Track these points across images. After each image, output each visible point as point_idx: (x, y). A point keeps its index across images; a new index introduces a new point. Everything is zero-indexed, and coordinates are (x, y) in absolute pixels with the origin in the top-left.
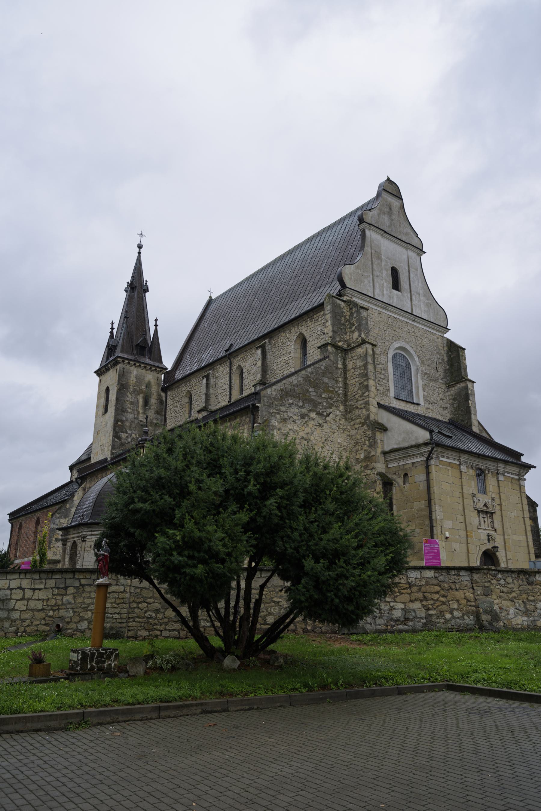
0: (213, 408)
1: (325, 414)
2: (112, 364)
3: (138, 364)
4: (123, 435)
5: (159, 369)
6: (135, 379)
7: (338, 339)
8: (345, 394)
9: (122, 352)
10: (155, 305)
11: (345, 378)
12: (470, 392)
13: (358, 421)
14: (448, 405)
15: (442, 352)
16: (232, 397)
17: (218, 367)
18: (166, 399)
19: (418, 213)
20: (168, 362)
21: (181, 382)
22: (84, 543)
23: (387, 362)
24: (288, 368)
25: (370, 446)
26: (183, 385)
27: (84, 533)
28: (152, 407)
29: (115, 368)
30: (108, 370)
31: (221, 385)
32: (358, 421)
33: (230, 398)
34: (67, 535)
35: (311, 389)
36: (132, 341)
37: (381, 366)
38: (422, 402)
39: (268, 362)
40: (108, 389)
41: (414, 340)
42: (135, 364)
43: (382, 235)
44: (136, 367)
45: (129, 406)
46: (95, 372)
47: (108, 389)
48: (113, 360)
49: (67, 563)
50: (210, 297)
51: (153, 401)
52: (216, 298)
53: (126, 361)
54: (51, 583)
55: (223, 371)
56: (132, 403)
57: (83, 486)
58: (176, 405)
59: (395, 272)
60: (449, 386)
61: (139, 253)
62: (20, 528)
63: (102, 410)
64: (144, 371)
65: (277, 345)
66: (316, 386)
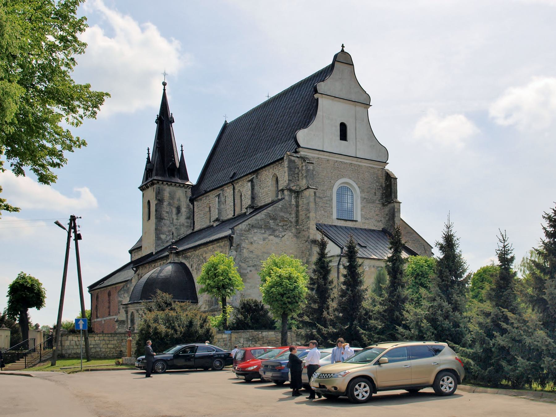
1: (281, 236)
3: (170, 183)
4: (163, 237)
6: (168, 195)
7: (293, 185)
8: (297, 222)
9: (157, 175)
11: (298, 211)
12: (396, 210)
13: (303, 239)
14: (383, 219)
15: (381, 180)
18: (194, 208)
19: (366, 74)
20: (193, 178)
23: (331, 195)
25: (310, 255)
29: (153, 187)
30: (148, 187)
32: (303, 239)
35: (270, 221)
36: (164, 165)
37: (326, 198)
38: (359, 219)
39: (256, 191)
40: (149, 202)
41: (356, 175)
43: (332, 100)
44: (169, 185)
47: (149, 202)
48: (151, 181)
50: (226, 121)
51: (184, 210)
54: (116, 338)
55: (228, 191)
57: (137, 272)
58: (200, 212)
59: (343, 128)
60: (384, 205)
61: (164, 90)
62: (97, 297)
63: (147, 217)
64: (174, 188)
66: (274, 219)
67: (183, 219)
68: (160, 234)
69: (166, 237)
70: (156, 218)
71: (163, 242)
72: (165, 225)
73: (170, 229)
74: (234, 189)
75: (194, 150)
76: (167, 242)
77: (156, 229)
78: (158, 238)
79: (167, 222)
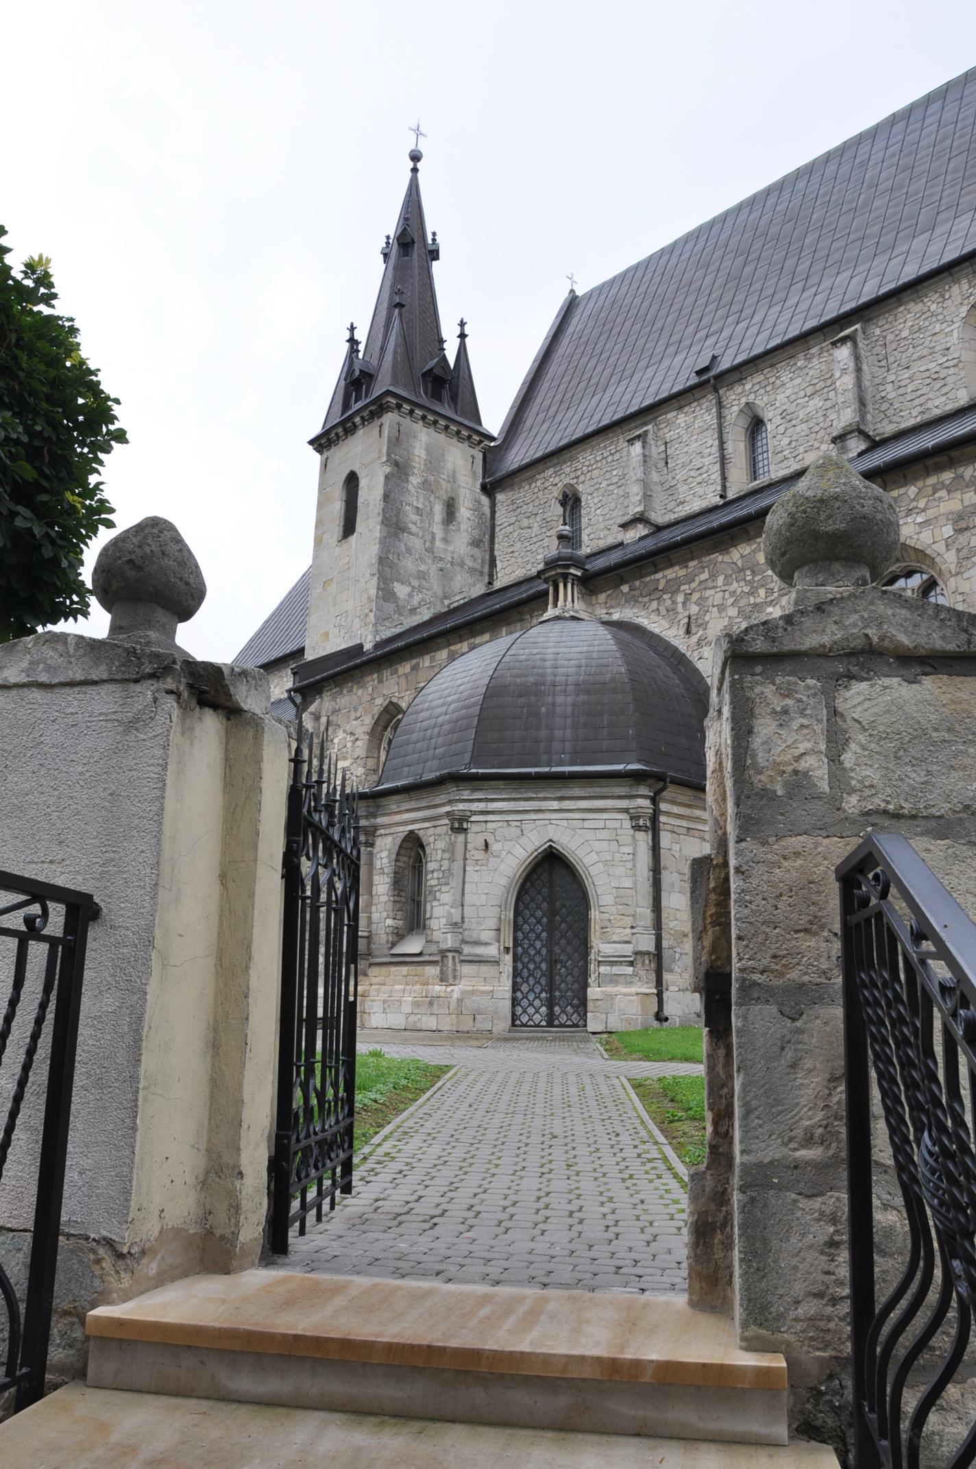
0: (659, 518)
2: (365, 414)
3: (432, 420)
4: (401, 590)
5: (476, 438)
6: (423, 454)
10: (455, 294)
16: (728, 485)
17: (669, 416)
18: (493, 512)
21: (541, 466)
22: (461, 838)
24: (944, 390)
26: (551, 471)
27: (461, 806)
28: (463, 527)
29: (377, 422)
31: (685, 459)
33: (724, 487)
34: (374, 816)
40: (352, 481)
42: (362, 418)
45: (415, 518)
46: (311, 442)
49: (384, 899)
50: (572, 291)
52: (590, 294)
53: (406, 407)
56: (418, 511)
61: (415, 170)
63: (336, 528)
64: (442, 437)
65: (890, 337)
67: (460, 544)
68: (392, 581)
69: (410, 595)
70: (386, 522)
71: (399, 610)
72: (409, 551)
73: (423, 568)
74: (720, 405)
75: (498, 340)
76: (413, 611)
77: (381, 560)
78: (386, 594)
79: (416, 543)
